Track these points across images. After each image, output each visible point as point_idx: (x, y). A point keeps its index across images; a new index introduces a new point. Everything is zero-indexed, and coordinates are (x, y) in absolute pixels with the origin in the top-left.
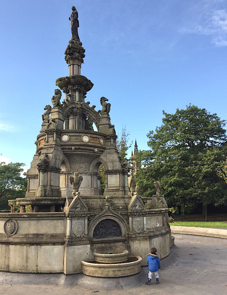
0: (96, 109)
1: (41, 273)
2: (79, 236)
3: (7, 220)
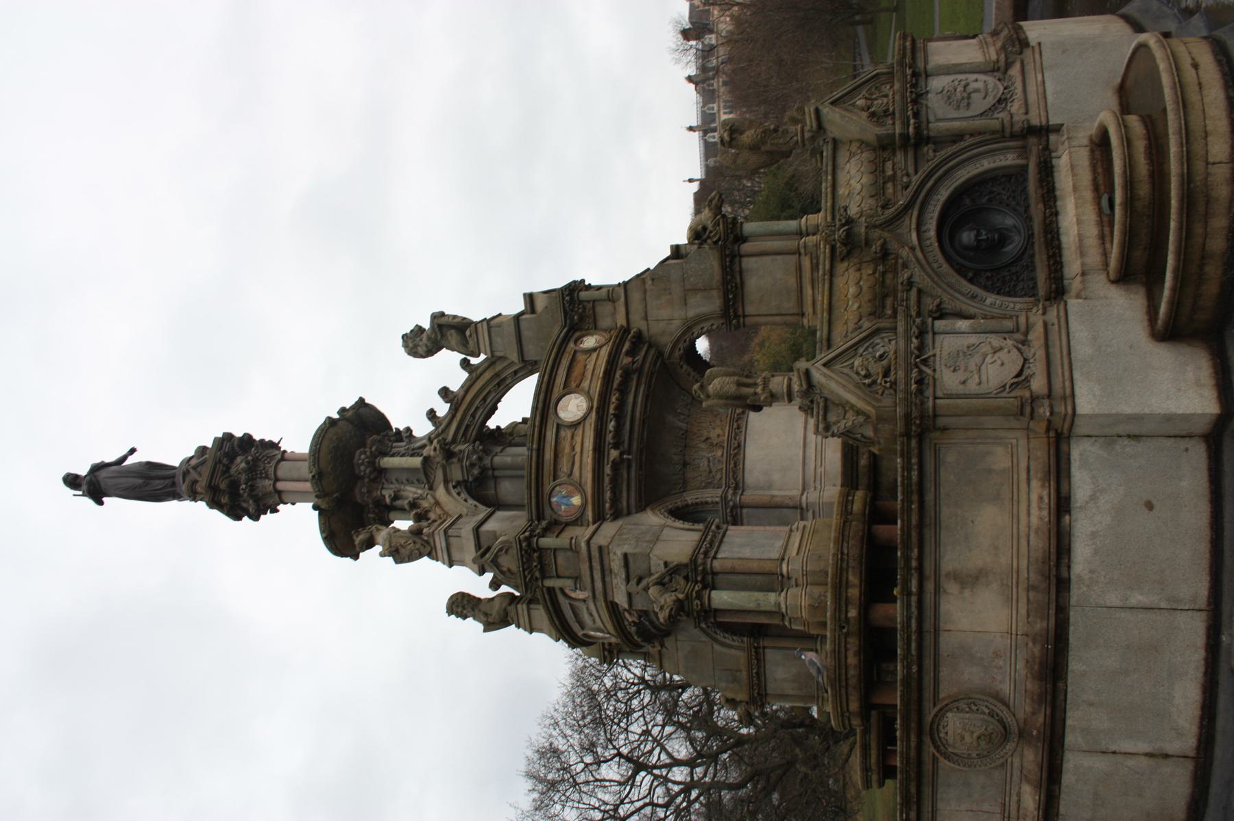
3: (932, 749)
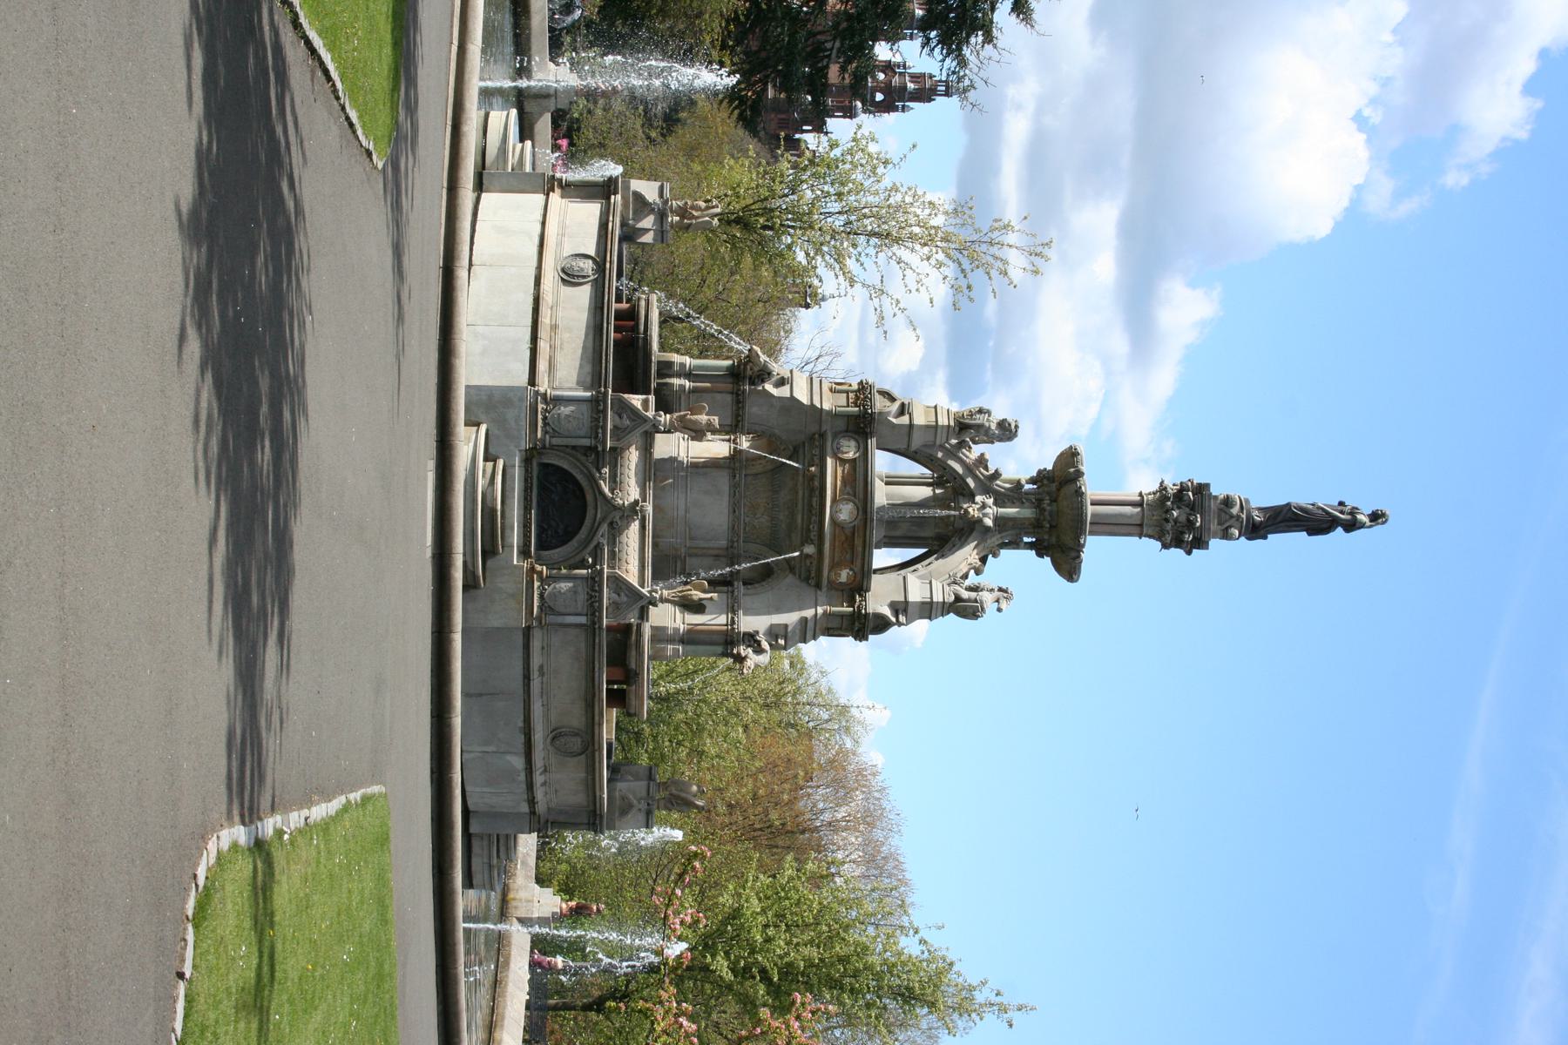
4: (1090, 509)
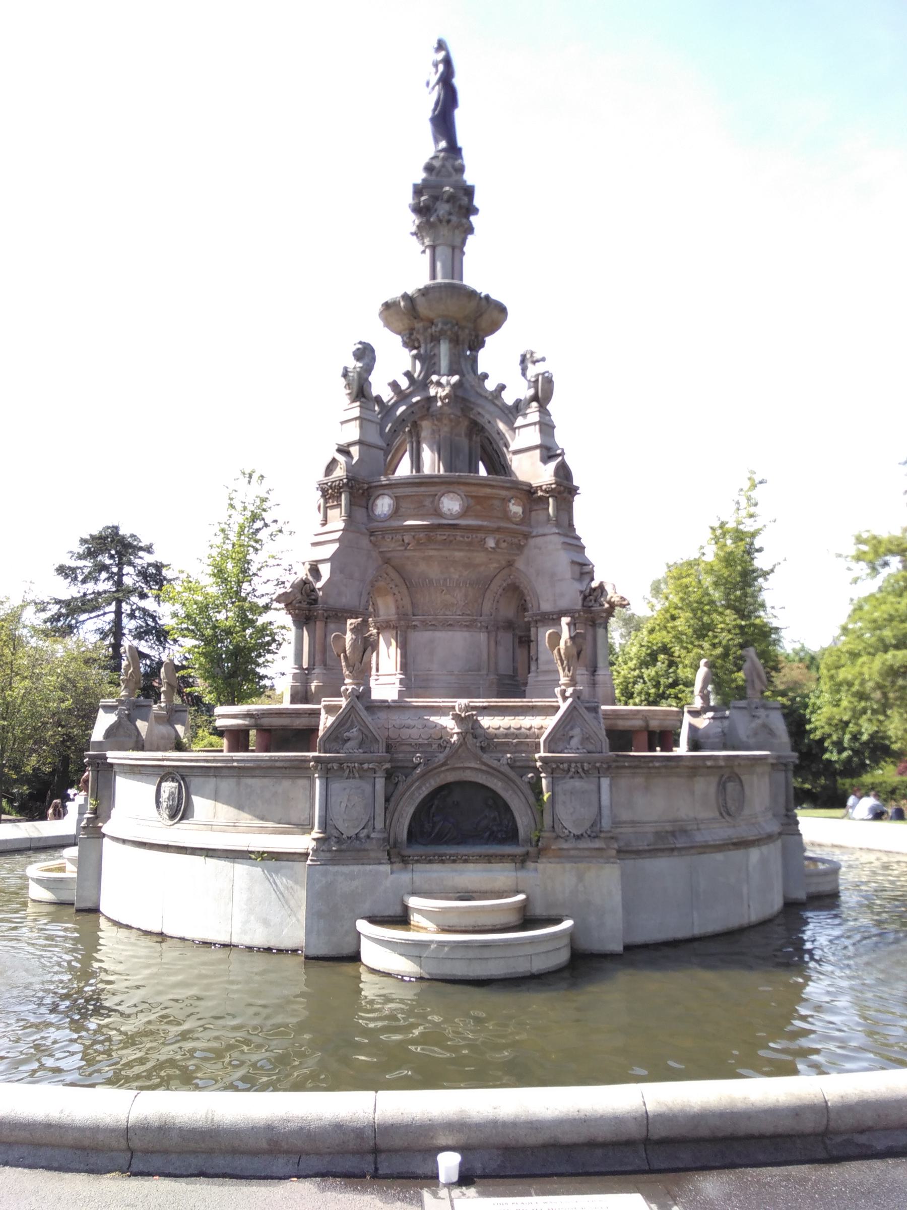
0: (509, 398)
1: (645, 946)
2: (352, 833)
4: (439, 280)
